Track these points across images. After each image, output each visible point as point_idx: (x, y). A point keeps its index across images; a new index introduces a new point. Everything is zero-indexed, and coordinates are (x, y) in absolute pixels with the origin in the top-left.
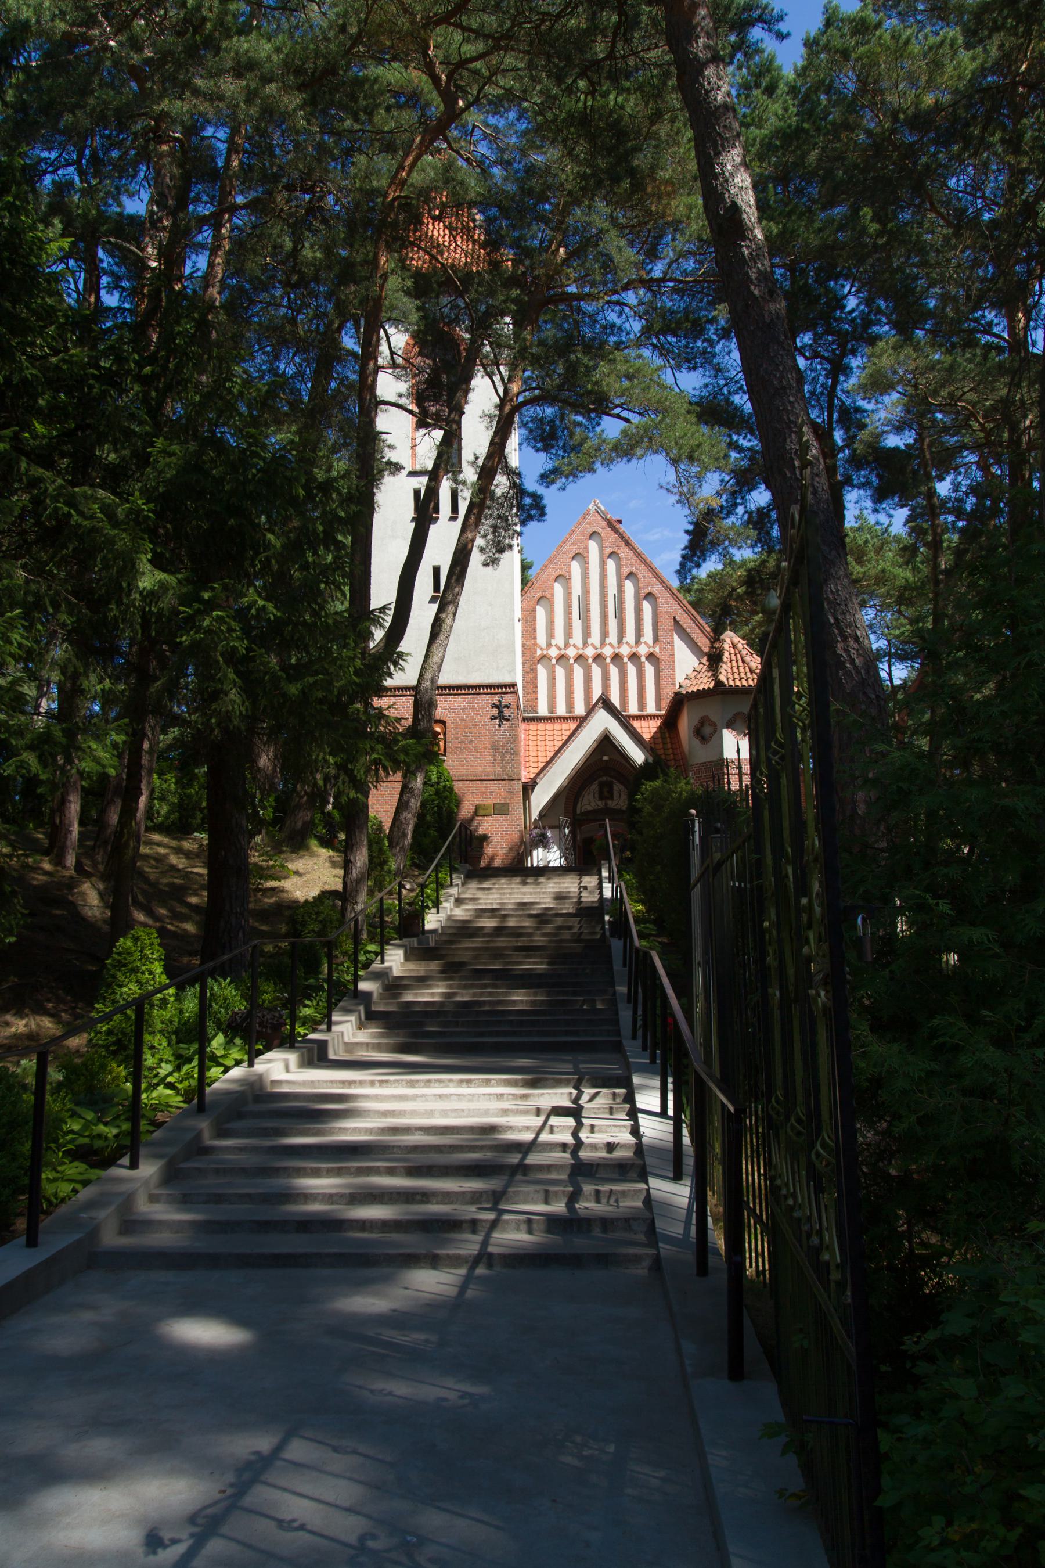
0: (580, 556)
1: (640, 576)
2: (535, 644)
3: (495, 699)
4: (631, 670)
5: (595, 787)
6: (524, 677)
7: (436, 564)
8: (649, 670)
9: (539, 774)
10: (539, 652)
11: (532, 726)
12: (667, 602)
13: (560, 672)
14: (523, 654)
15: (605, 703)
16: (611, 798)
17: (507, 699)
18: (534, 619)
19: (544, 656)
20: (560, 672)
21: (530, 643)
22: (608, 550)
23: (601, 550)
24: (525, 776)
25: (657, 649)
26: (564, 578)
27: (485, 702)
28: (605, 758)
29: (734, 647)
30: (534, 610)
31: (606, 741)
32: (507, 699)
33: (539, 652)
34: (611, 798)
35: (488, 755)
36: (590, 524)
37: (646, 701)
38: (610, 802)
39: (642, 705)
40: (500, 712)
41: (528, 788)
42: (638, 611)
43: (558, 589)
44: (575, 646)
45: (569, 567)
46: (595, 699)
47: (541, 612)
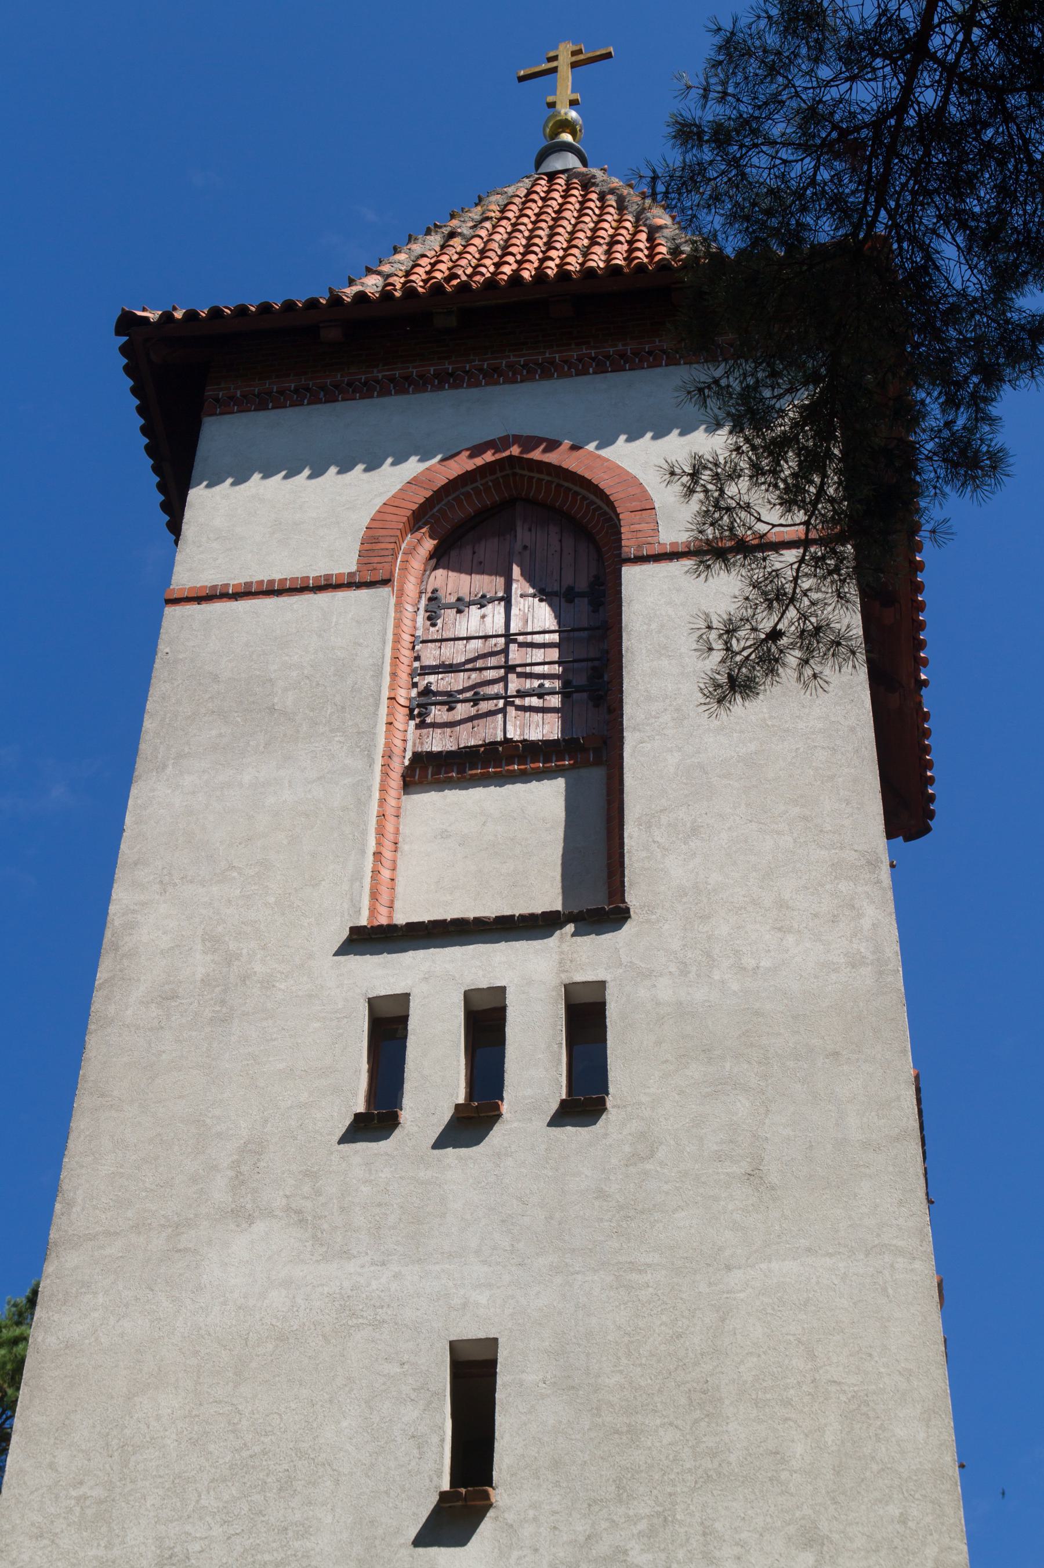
7: (472, 1330)
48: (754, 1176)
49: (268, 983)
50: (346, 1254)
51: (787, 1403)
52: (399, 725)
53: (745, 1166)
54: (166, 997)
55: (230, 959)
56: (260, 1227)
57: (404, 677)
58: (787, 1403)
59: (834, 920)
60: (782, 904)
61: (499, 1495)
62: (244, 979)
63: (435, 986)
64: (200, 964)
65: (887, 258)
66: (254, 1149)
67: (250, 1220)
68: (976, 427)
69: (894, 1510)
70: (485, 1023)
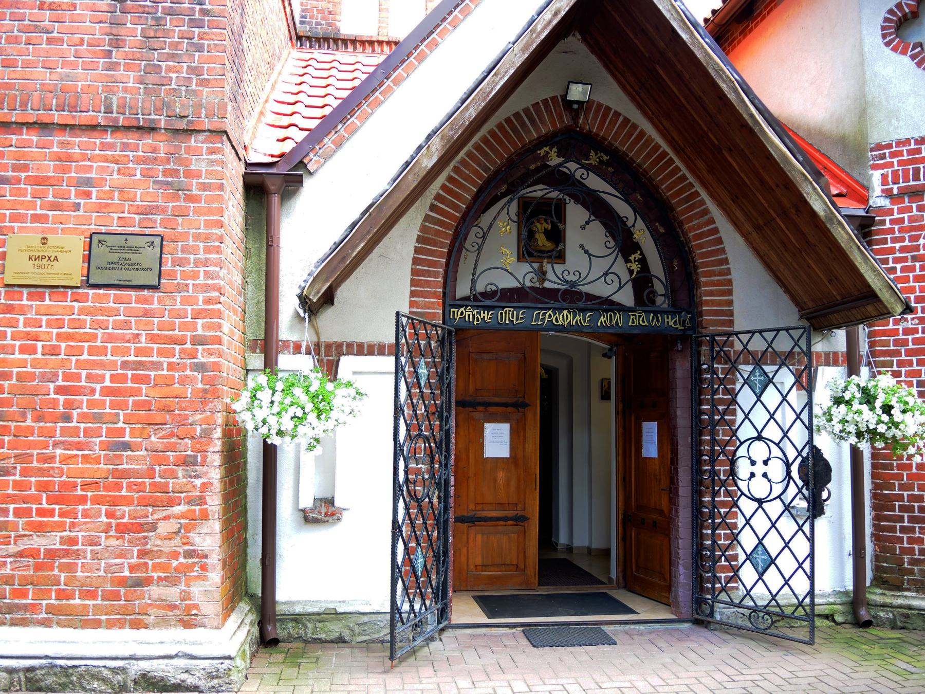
28: (577, 92)
41: (267, 189)
61: (223, 629)
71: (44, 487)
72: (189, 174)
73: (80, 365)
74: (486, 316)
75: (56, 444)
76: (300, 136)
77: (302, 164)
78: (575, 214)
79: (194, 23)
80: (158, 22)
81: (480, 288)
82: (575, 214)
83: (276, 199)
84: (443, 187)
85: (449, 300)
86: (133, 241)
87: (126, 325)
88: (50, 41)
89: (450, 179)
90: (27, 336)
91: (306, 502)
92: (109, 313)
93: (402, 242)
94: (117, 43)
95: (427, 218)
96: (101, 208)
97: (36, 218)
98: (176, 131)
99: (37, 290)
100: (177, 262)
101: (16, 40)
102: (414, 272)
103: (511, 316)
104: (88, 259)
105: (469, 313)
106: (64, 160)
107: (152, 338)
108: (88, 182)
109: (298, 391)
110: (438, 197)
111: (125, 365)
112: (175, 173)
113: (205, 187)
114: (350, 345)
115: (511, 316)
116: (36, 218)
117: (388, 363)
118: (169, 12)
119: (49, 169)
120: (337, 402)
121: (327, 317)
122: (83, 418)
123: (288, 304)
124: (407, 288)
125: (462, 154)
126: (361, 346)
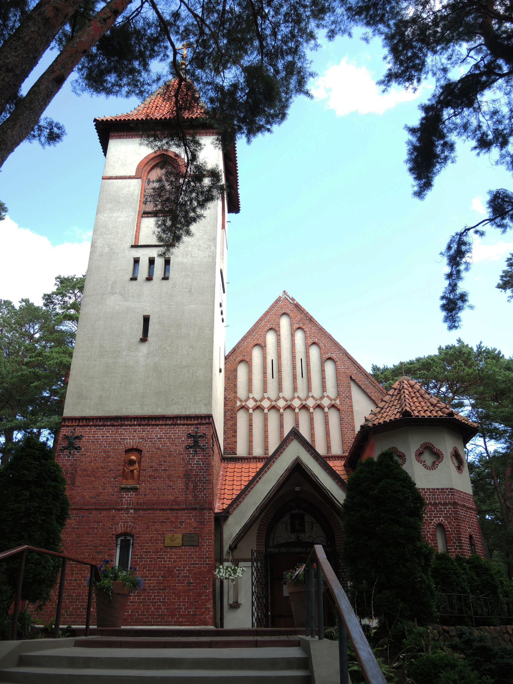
0: (276, 330)
1: (321, 345)
2: (236, 397)
3: (191, 430)
4: (318, 416)
5: (287, 518)
6: (225, 423)
7: (146, 314)
8: (334, 417)
9: (231, 505)
10: (239, 403)
11: (231, 465)
12: (344, 364)
13: (257, 417)
14: (225, 405)
15: (295, 434)
16: (303, 531)
17: (202, 429)
18: (236, 377)
19: (242, 407)
20: (257, 417)
21: (231, 396)
22: (296, 326)
23: (291, 325)
24: (218, 507)
25: (338, 402)
26: (263, 346)
27: (181, 433)
28: (297, 489)
29: (412, 387)
30: (235, 370)
31: (298, 468)
32: (202, 429)
33: (239, 403)
34: (303, 531)
35: (180, 484)
36: (281, 307)
37: (331, 438)
38: (302, 535)
39: (329, 448)
40: (196, 442)
41: (221, 519)
42: (323, 371)
43: (256, 353)
44: (269, 399)
45: (265, 338)
46: (286, 434)
47: (242, 371)
48: (190, 291)
49: (117, 254)
50: (128, 301)
51: (191, 327)
52: (141, 206)
53: (189, 290)
54: (101, 255)
55: (112, 249)
56: (115, 295)
57: (143, 196)
58: (191, 327)
59: (207, 249)
60: (199, 246)
62: (114, 253)
63: (144, 255)
64: (107, 250)
65: (23, 310)
66: (115, 283)
67: (114, 294)
68: (156, 28)
69: (204, 343)
70: (152, 261)
71: (173, 593)
72: (204, 519)
73: (181, 564)
74: (277, 550)
75: (176, 583)
76: (229, 502)
77: (228, 512)
78: (308, 519)
79: (205, 483)
80: (197, 483)
81: (275, 544)
82: (308, 519)
83: (222, 522)
84: (264, 516)
85: (267, 546)
86: (192, 535)
87: (191, 555)
88: (172, 489)
89: (266, 513)
90: (170, 558)
91: (231, 602)
92: (187, 552)
93: (254, 531)
94: (187, 489)
95: (260, 524)
96: (185, 528)
97: (171, 531)
98: (201, 509)
99: (172, 547)
100: (202, 540)
101: (165, 489)
102: (257, 539)
103: (283, 550)
104: (183, 540)
105: (272, 550)
106: (176, 517)
107: (197, 558)
108: (183, 522)
109: (229, 569)
110: (263, 519)
111: (191, 564)
112: (201, 519)
113: (208, 522)
114: (241, 559)
115: (283, 550)
116: (171, 531)
117: (250, 564)
118: (198, 481)
119: (173, 519)
120: (238, 571)
121: (236, 551)
122: (182, 577)
123: (226, 548)
124: (256, 543)
125: (269, 507)
126: (244, 559)
